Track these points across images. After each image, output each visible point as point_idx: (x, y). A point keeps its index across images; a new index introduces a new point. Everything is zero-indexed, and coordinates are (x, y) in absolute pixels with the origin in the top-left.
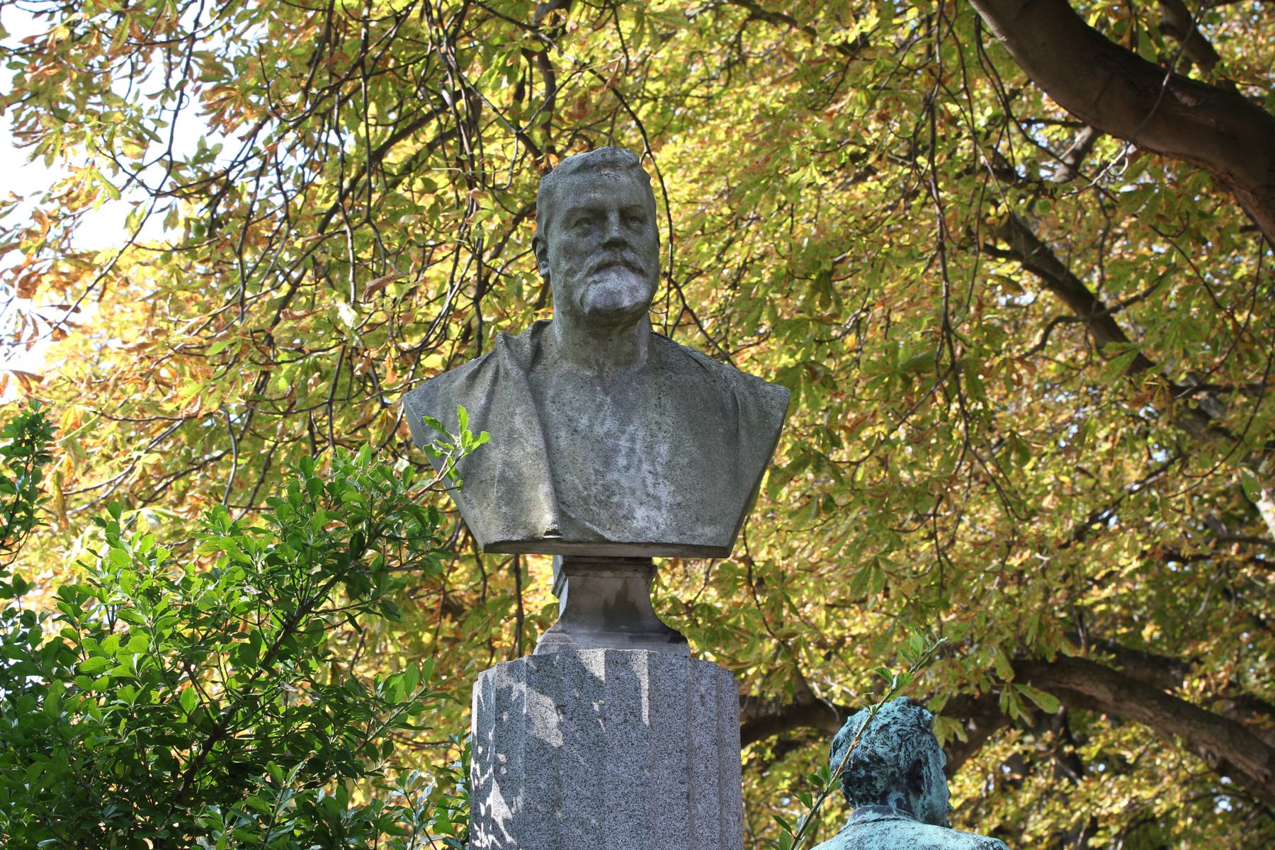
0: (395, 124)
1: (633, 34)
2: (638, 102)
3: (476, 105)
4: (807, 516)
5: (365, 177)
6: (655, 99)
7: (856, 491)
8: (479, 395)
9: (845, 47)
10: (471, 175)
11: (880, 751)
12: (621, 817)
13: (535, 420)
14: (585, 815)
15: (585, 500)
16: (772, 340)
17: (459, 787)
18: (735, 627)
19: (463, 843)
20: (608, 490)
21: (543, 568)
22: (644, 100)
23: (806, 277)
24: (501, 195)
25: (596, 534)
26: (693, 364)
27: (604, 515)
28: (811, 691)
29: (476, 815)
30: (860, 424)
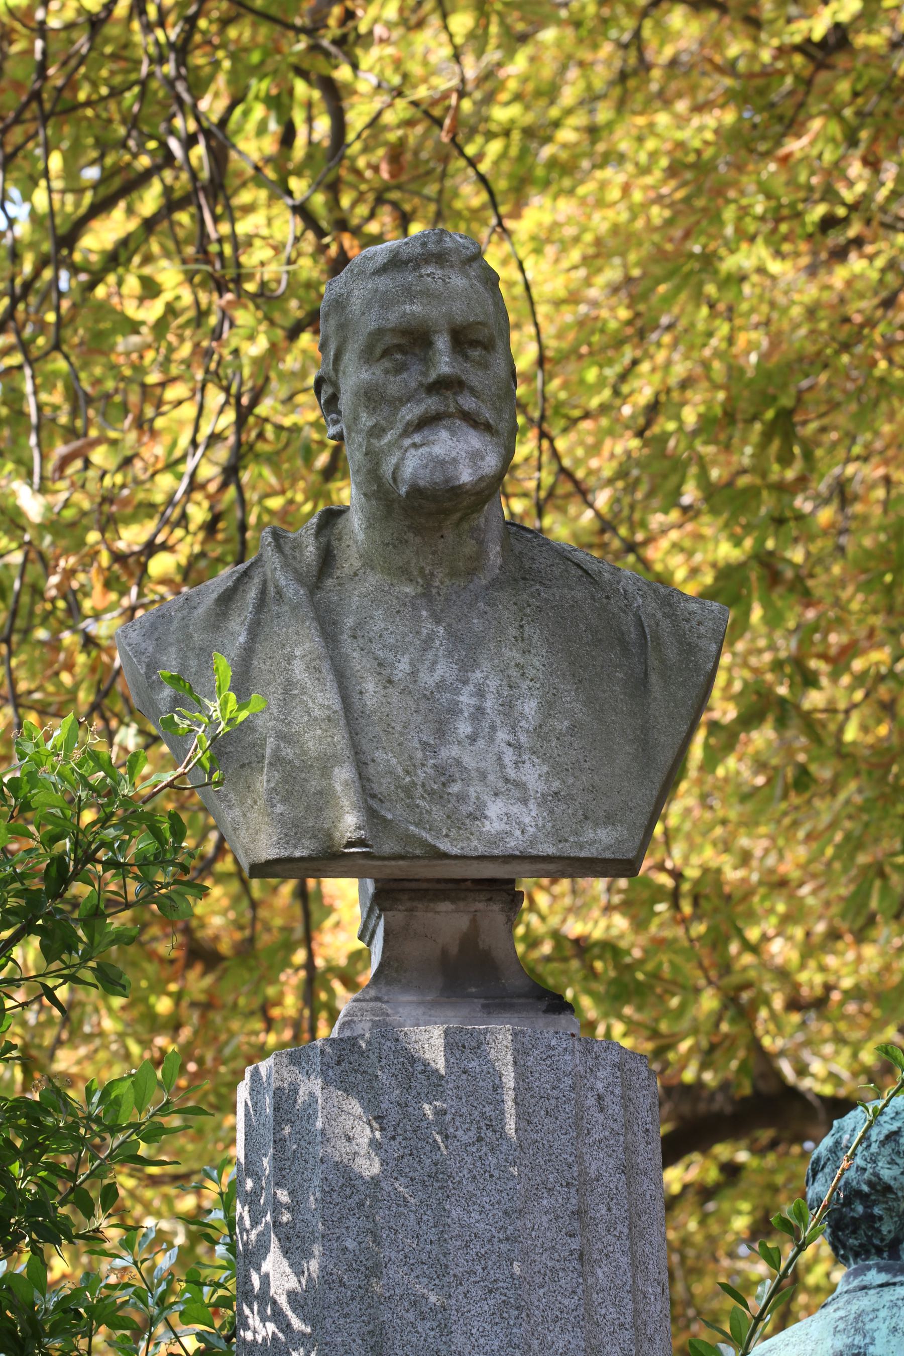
0: (95, 186)
1: (471, 36)
2: (479, 139)
3: (219, 154)
4: (769, 800)
5: (47, 274)
6: (507, 133)
7: (841, 752)
8: (238, 629)
9: (806, 47)
10: (220, 273)
11: (887, 1174)
12: (477, 1292)
13: (326, 666)
14: (420, 1289)
15: (408, 791)
16: (706, 519)
17: (220, 1249)
18: (656, 976)
19: (228, 1339)
20: (445, 775)
21: (345, 894)
22: (490, 136)
23: (755, 418)
24: (265, 298)
25: (424, 844)
26: (574, 571)
27: (438, 814)
28: (778, 1075)
29: (246, 1294)
30: (850, 651)
